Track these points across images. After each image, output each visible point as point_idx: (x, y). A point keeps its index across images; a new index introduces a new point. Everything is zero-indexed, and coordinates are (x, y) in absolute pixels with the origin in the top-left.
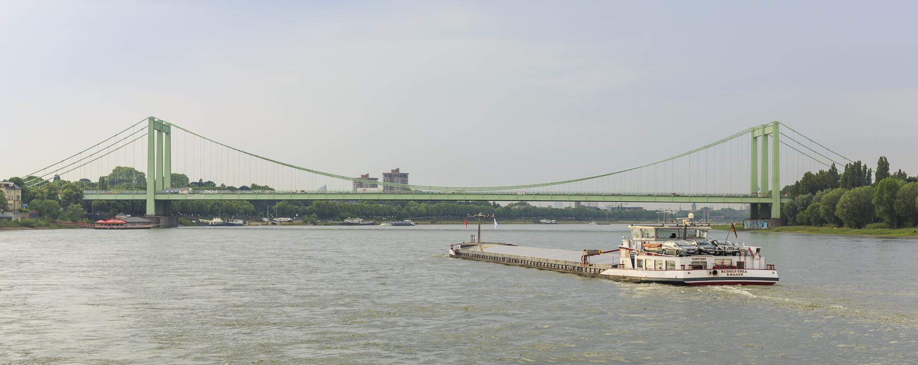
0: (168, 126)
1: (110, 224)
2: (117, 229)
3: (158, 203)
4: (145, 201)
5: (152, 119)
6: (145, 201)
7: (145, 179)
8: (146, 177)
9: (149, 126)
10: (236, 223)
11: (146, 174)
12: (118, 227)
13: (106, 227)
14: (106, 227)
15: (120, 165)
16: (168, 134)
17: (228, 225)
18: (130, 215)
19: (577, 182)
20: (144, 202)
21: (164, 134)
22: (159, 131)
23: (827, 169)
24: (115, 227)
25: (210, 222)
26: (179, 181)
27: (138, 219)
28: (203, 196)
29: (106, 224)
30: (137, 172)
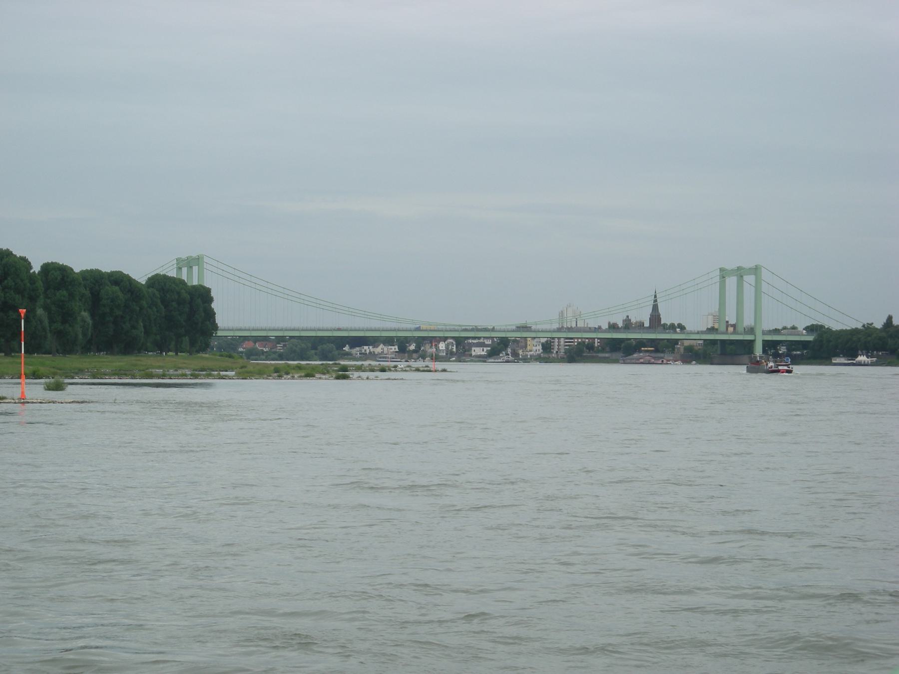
20: (751, 343)
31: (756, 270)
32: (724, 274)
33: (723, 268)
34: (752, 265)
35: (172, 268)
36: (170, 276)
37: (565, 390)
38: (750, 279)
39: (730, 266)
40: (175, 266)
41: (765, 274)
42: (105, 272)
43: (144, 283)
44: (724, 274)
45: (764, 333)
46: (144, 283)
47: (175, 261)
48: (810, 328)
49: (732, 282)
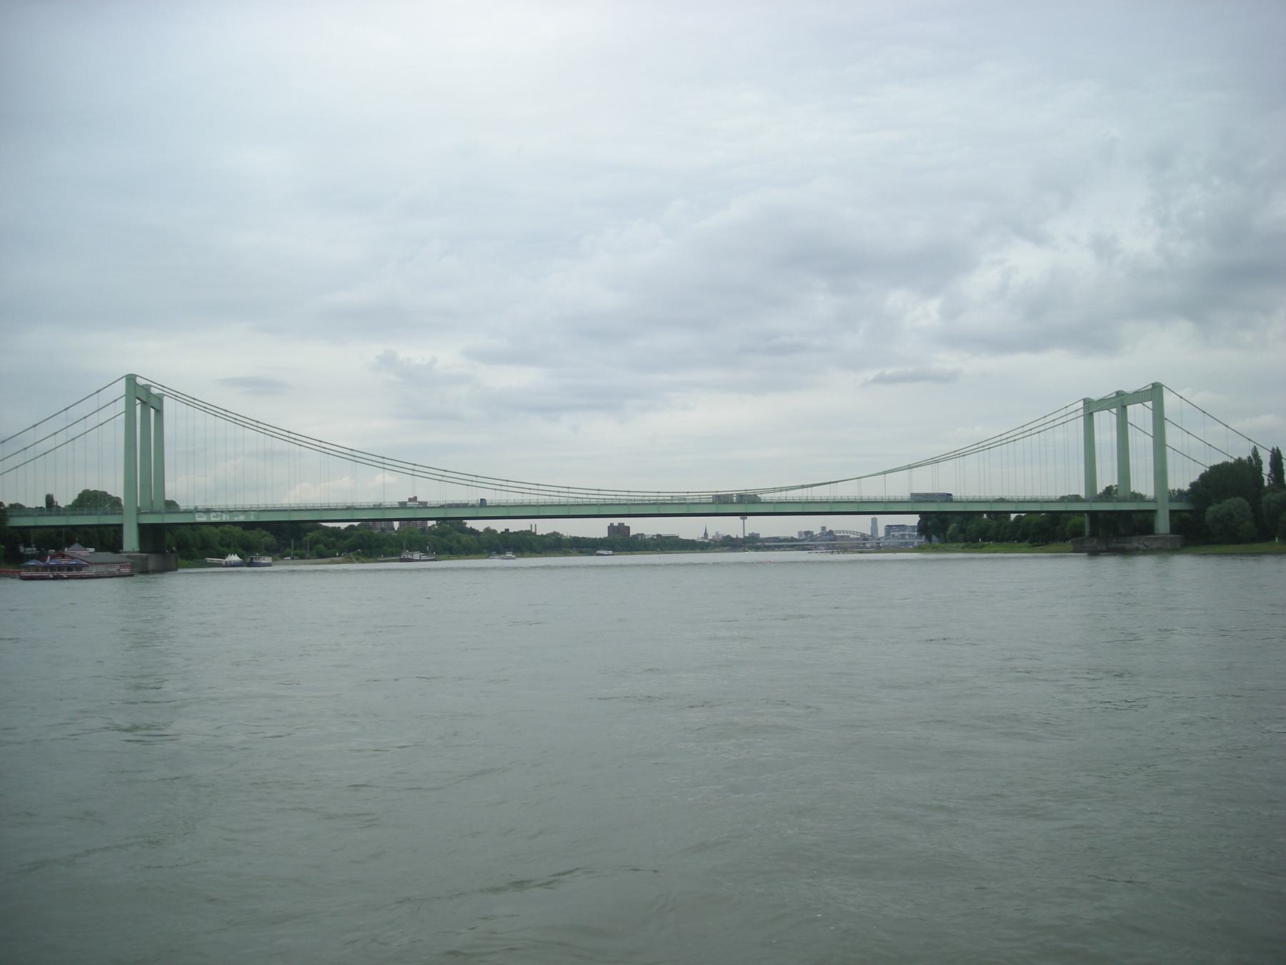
0: (160, 398)
1: (52, 568)
2: (69, 578)
3: (144, 530)
4: (120, 526)
5: (131, 379)
6: (120, 526)
7: (121, 505)
8: (123, 503)
9: (127, 395)
10: (263, 562)
11: (122, 498)
12: (70, 574)
13: (44, 574)
14: (44, 574)
15: (88, 488)
16: (159, 412)
17: (250, 565)
18: (93, 549)
19: (814, 488)
20: (119, 528)
21: (152, 411)
22: (143, 403)
23: (1245, 455)
24: (64, 574)
25: (1128, 546)
26: (171, 506)
27: (107, 556)
28: (224, 516)
29: (45, 568)
30: (110, 497)
31: (1154, 393)
32: (1090, 408)
33: (1088, 399)
34: (1142, 383)
35: (1074, 415)
36: (1193, 485)
37: (1260, 669)
38: (1140, 414)
39: (1098, 392)
40: (1081, 412)
41: (1169, 400)
42: (66, 506)
43: (606, 535)
44: (1090, 408)
45: (139, 512)
46: (606, 535)
47: (1081, 404)
48: (113, 500)
49: (1105, 422)
